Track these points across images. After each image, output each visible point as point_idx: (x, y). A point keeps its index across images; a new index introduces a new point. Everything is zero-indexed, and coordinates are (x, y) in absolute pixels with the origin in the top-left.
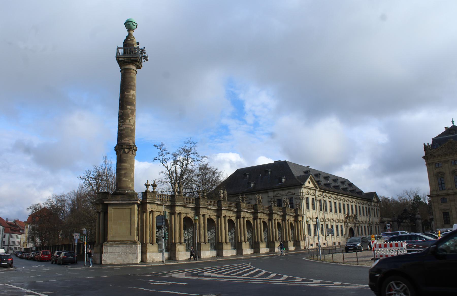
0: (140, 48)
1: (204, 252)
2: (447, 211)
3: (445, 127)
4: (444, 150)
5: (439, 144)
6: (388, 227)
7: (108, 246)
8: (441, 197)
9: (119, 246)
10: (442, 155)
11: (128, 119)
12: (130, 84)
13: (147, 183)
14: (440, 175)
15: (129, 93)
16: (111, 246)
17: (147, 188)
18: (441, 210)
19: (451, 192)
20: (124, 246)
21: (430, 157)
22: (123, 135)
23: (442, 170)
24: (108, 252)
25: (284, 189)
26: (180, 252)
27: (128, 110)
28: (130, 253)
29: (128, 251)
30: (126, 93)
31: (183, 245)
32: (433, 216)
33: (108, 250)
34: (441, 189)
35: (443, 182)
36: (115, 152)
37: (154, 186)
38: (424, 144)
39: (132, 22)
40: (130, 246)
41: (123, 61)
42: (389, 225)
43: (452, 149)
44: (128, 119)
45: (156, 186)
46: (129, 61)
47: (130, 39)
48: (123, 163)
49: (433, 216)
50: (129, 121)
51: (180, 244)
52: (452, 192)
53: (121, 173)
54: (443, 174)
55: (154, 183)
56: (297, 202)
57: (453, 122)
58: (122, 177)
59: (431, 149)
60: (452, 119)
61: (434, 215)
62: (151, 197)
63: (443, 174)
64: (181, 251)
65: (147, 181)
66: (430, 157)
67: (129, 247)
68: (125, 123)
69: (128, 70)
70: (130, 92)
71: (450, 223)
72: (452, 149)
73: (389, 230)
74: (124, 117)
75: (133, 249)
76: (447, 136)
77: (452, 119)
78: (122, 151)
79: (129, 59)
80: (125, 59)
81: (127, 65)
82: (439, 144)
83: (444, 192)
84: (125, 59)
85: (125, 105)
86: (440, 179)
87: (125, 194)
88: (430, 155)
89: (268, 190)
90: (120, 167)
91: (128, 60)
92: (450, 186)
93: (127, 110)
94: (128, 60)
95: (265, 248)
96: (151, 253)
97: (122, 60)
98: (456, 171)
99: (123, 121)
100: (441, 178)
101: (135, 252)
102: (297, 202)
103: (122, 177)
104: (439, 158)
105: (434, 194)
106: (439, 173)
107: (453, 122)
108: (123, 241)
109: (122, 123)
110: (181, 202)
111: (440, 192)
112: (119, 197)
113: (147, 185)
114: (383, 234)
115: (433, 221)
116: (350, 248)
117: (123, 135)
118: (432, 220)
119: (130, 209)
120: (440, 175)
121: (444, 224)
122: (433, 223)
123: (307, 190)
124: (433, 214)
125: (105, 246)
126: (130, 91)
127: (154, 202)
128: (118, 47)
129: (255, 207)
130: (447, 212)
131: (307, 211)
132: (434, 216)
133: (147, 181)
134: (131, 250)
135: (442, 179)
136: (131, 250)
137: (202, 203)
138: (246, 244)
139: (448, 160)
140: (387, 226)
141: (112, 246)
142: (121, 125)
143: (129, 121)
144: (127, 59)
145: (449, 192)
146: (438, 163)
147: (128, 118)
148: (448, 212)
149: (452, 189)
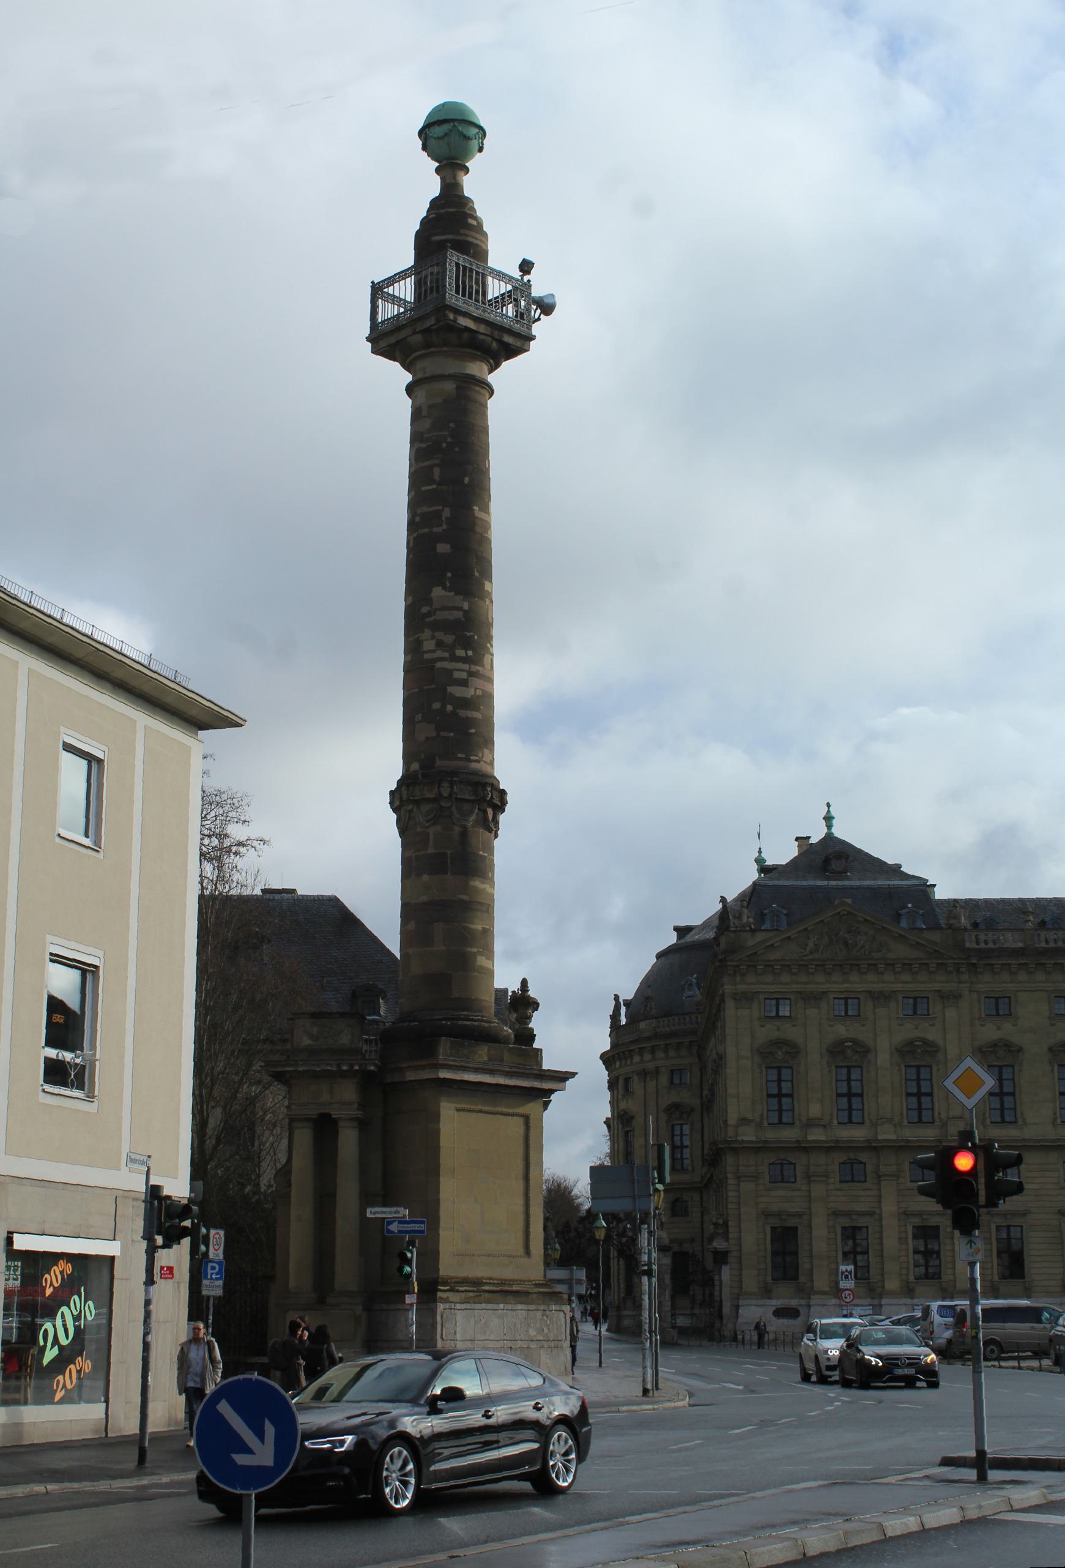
0: (536, 292)
2: (792, 1222)
3: (797, 839)
4: (811, 944)
5: (785, 912)
6: (847, 1277)
7: (458, 1306)
8: (841, 1157)
9: (502, 1306)
10: (800, 965)
14: (780, 1055)
16: (468, 1306)
18: (766, 1214)
19: (816, 1135)
20: (520, 1307)
21: (748, 966)
22: (473, 731)
23: (791, 1032)
24: (458, 1337)
28: (543, 1347)
29: (532, 1333)
32: (727, 1240)
33: (458, 1330)
34: (914, 1116)
35: (856, 1087)
38: (723, 900)
39: (453, 120)
40: (542, 1307)
41: (466, 335)
42: (850, 1272)
43: (846, 944)
46: (494, 344)
49: (727, 1240)
52: (823, 1138)
53: (472, 926)
54: (793, 1050)
57: (828, 819)
58: (475, 950)
59: (753, 931)
60: (828, 805)
61: (731, 1236)
63: (793, 1050)
66: (748, 966)
67: (539, 1314)
68: (478, 671)
69: (477, 388)
71: (796, 1278)
72: (846, 944)
73: (847, 1292)
74: (476, 637)
75: (551, 1326)
76: (819, 883)
77: (828, 805)
78: (473, 817)
79: (496, 334)
80: (482, 328)
81: (474, 358)
82: (785, 912)
83: (789, 1134)
84: (482, 328)
85: (477, 574)
86: (775, 1071)
88: (748, 956)
90: (465, 897)
91: (493, 338)
92: (815, 1110)
94: (493, 338)
97: (467, 329)
98: (848, 1047)
99: (470, 653)
100: (779, 1069)
101: (561, 1340)
103: (475, 950)
104: (785, 978)
105: (745, 1138)
106: (778, 1043)
107: (828, 819)
108: (510, 1282)
109: (466, 667)
111: (770, 1135)
112: (483, 1053)
114: (940, 1307)
115: (726, 1263)
116: (1029, 1354)
117: (473, 731)
118: (721, 1257)
119: (521, 1120)
120: (780, 1055)
121: (769, 1279)
122: (726, 1274)
124: (727, 1232)
125: (447, 1305)
130: (789, 1225)
132: (732, 1242)
134: (546, 1330)
135: (786, 1074)
136: (546, 1330)
139: (823, 992)
140: (843, 1273)
141: (472, 1306)
142: (464, 675)
144: (488, 331)
145: (810, 1138)
146: (778, 999)
148: (795, 1229)
149: (824, 1126)
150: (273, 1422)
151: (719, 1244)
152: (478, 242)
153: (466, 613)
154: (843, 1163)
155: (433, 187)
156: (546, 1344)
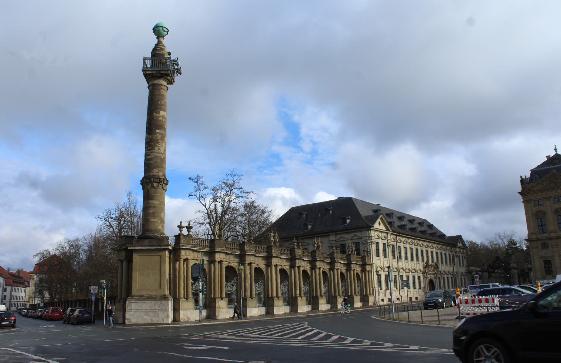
0: (172, 59)
1: (250, 309)
2: (549, 259)
3: (546, 156)
4: (545, 184)
5: (539, 177)
6: (477, 278)
7: (133, 302)
8: (541, 242)
9: (147, 302)
10: (542, 190)
11: (157, 146)
12: (160, 103)
13: (180, 224)
14: (540, 215)
15: (158, 114)
16: (136, 302)
17: (181, 231)
18: (542, 257)
19: (553, 235)
20: (153, 301)
22: (151, 166)
23: (542, 208)
24: (133, 309)
25: (349, 232)
26: (221, 309)
27: (157, 135)
29: (157, 307)
30: (154, 114)
31: (225, 301)
32: (531, 265)
33: (133, 307)
34: (541, 231)
35: (543, 223)
36: (141, 186)
37: (189, 228)
38: (521, 177)
39: (162, 27)
41: (151, 75)
42: (478, 277)
43: (555, 182)
44: (157, 146)
45: (191, 228)
46: (159, 75)
47: (160, 47)
48: (151, 200)
49: (531, 265)
50: (159, 149)
51: (221, 299)
52: (555, 235)
53: (149, 212)
54: (544, 213)
55: (189, 224)
56: (364, 248)
57: (556, 149)
58: (150, 217)
59: (528, 183)
60: (555, 146)
61: (532, 264)
62: (185, 242)
63: (544, 213)
64: (222, 308)
65: (181, 222)
67: (159, 303)
68: (153, 151)
69: (157, 86)
70: (159, 113)
71: (552, 274)
72: (555, 182)
73: (477, 282)
76: (549, 167)
77: (555, 146)
78: (150, 186)
79: (158, 72)
80: (154, 72)
81: (156, 79)
82: (539, 177)
83: (545, 235)
84: (154, 72)
85: (154, 129)
86: (540, 219)
87: (153, 238)
88: (527, 190)
89: (330, 234)
90: (148, 205)
91: (158, 73)
92: (552, 228)
93: (156, 134)
94: (158, 73)
95: (325, 304)
96: (186, 310)
97: (150, 74)
98: (559, 210)
99: (151, 148)
100: (541, 219)
102: (364, 248)
103: (150, 217)
104: (539, 194)
105: (533, 238)
106: (539, 212)
107: (556, 149)
108: (151, 296)
109: (150, 151)
110: (222, 247)
111: (540, 236)
113: (181, 227)
114: (470, 287)
115: (532, 271)
117: (151, 166)
118: (530, 269)
119: (159, 257)
120: (540, 215)
121: (544, 274)
122: (532, 273)
123: (376, 233)
124: (531, 263)
125: (129, 302)
126: (160, 112)
127: (189, 248)
128: (145, 57)
129: (313, 254)
130: (548, 260)
131: (377, 259)
132: (533, 265)
133: (181, 222)
134: (161, 307)
135: (543, 220)
136: (161, 307)
137: (248, 249)
138: (301, 299)
139: (550, 197)
140: (475, 277)
141: (137, 302)
142: (149, 153)
143: (159, 148)
144: (156, 72)
145: (551, 236)
146: (538, 200)
147: (157, 145)
148: (550, 260)
149: (555, 232)
150: (372, 316)
151: (529, 266)
152: (159, 53)
153: (150, 138)
154: (542, 244)
155: (156, 41)
156: (161, 310)
